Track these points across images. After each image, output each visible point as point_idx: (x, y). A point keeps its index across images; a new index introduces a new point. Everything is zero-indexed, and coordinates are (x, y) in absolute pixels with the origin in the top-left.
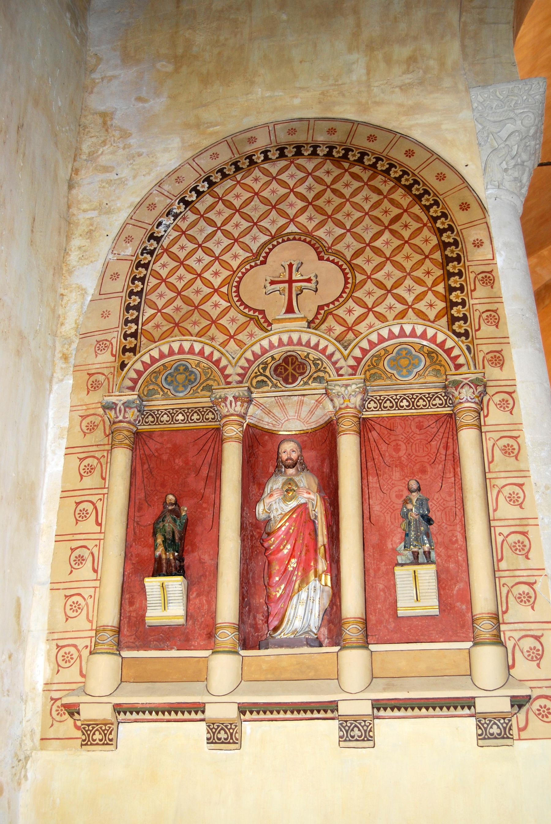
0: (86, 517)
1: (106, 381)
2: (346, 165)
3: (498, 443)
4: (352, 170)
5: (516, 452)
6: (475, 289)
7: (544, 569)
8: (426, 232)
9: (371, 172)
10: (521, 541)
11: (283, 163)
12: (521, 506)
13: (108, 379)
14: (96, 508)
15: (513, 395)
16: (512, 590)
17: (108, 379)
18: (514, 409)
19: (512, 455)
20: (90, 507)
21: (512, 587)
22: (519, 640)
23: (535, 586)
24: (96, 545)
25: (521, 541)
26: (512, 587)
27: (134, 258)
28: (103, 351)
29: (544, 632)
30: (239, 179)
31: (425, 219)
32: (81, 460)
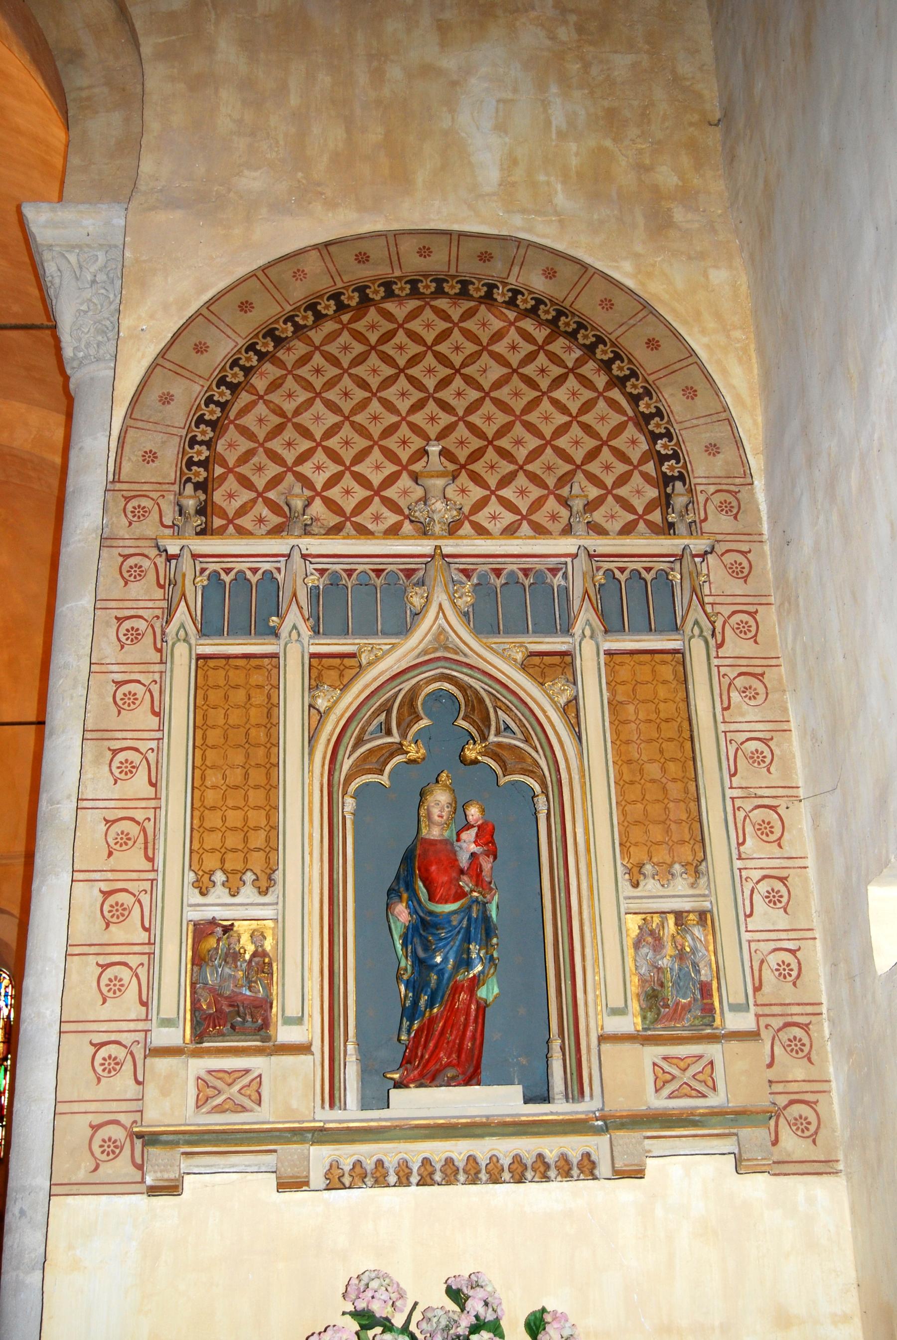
0: (123, 915)
1: (150, 630)
2: (511, 315)
3: (737, 682)
4: (520, 324)
5: (813, 1128)
6: (706, 519)
7: (812, 930)
8: (631, 431)
9: (549, 331)
10: (728, 501)
11: (412, 304)
12: (779, 842)
13: (152, 627)
14: (144, 830)
15: (770, 743)
16: (768, 958)
17: (152, 627)
18: (759, 635)
19: (789, 979)
20: (133, 830)
21: (734, 679)
22: (729, 617)
23: (798, 954)
24: (142, 964)
25: (728, 501)
26: (734, 679)
27: (184, 432)
28: (130, 775)
29: (759, 607)
30: (345, 322)
31: (630, 413)
32: (109, 823)
